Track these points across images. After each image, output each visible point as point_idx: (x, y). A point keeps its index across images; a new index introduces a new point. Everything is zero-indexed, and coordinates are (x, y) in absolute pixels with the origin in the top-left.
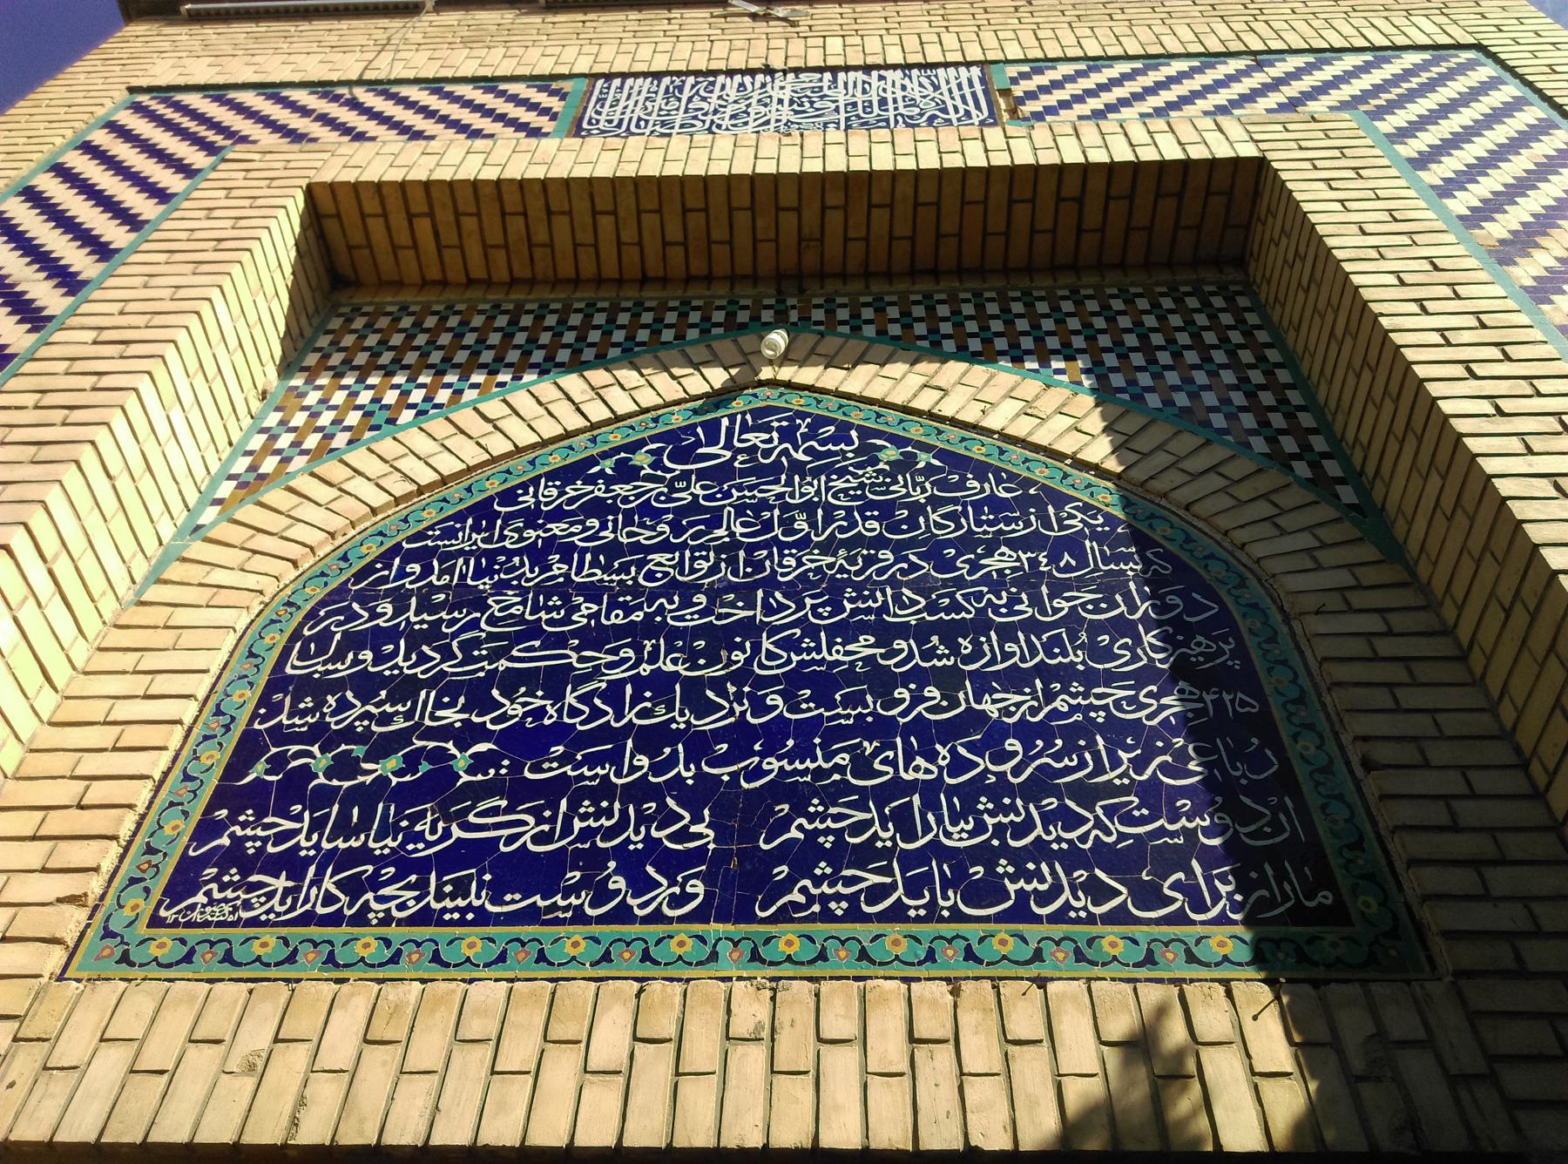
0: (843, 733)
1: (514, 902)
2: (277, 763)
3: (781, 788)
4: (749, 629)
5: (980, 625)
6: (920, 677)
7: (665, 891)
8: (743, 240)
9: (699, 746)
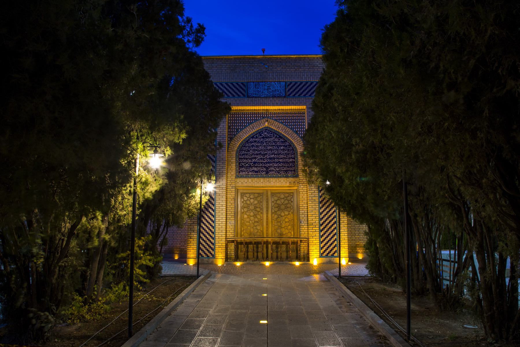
0: (272, 163)
1: (256, 174)
3: (269, 166)
4: (266, 154)
5: (280, 154)
6: (276, 158)
7: (263, 173)
8: (238, 100)
9: (264, 163)
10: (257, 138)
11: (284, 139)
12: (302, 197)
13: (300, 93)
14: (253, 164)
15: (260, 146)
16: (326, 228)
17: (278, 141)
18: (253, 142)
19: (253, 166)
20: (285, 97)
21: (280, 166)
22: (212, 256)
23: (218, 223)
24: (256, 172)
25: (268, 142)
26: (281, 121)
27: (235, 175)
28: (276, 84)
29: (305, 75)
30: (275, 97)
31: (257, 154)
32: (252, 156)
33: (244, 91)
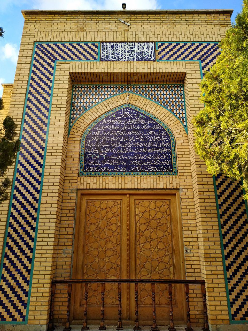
3: (131, 159)
4: (127, 141)
5: (148, 141)
6: (143, 147)
7: (123, 169)
8: (86, 65)
9: (124, 155)
10: (113, 119)
11: (155, 121)
12: (185, 207)
13: (176, 55)
14: (106, 156)
15: (118, 130)
16: (235, 263)
17: (145, 124)
18: (107, 125)
19: (106, 159)
20: (154, 61)
21: (149, 159)
22: (21, 319)
23: (40, 252)
24: (111, 167)
25: (130, 124)
26: (149, 97)
27: (77, 172)
28: (141, 45)
29: (183, 34)
30: (141, 60)
31: (114, 142)
32: (105, 144)
33: (96, 53)
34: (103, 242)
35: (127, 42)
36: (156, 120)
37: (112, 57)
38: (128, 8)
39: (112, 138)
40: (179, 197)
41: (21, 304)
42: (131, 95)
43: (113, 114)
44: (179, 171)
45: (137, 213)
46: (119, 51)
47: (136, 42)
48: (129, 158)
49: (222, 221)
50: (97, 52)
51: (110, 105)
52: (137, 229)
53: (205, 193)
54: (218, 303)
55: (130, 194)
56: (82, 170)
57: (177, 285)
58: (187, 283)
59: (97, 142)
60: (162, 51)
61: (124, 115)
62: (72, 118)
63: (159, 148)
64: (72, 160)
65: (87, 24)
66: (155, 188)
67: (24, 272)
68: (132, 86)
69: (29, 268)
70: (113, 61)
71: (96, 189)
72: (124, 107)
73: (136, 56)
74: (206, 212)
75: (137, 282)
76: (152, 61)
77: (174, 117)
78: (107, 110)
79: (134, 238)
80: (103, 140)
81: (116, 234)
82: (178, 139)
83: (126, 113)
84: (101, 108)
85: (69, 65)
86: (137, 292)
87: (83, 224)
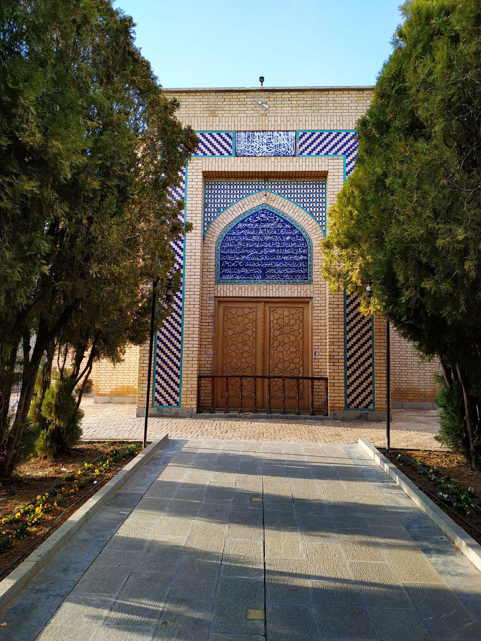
2: (224, 263)
3: (267, 267)
5: (285, 248)
8: (220, 161)
10: (249, 222)
14: (241, 264)
15: (254, 235)
17: (282, 228)
18: (242, 229)
19: (242, 267)
20: (294, 156)
23: (187, 352)
24: (248, 275)
27: (214, 279)
28: (280, 135)
30: (279, 156)
31: (249, 248)
32: (240, 251)
33: (230, 145)
34: (240, 345)
35: (265, 131)
36: (293, 224)
37: (248, 151)
38: (267, 85)
39: (248, 244)
40: (312, 305)
41: (174, 393)
42: (268, 194)
43: (249, 217)
44: (314, 280)
45: (272, 319)
46: (255, 143)
47: (275, 131)
48: (264, 265)
49: (348, 328)
50: (231, 144)
51: (245, 206)
52: (271, 334)
53: (335, 303)
54: (337, 395)
55: (265, 302)
56: (219, 278)
57: (306, 381)
58: (313, 379)
59: (233, 248)
60: (304, 142)
61: (261, 218)
62: (206, 222)
63: (295, 255)
64: (208, 267)
65: (219, 106)
66: (290, 296)
67: (175, 368)
68: (270, 183)
69: (179, 366)
70: (249, 156)
71: (232, 297)
72: (260, 208)
73: (274, 150)
74: (333, 320)
75: (269, 378)
76: (291, 156)
77: (313, 220)
78: (242, 213)
79: (268, 343)
80: (239, 246)
81: (251, 338)
82: (316, 245)
83: (263, 215)
84: (236, 210)
85: (201, 161)
86: (269, 386)
87: (221, 329)
